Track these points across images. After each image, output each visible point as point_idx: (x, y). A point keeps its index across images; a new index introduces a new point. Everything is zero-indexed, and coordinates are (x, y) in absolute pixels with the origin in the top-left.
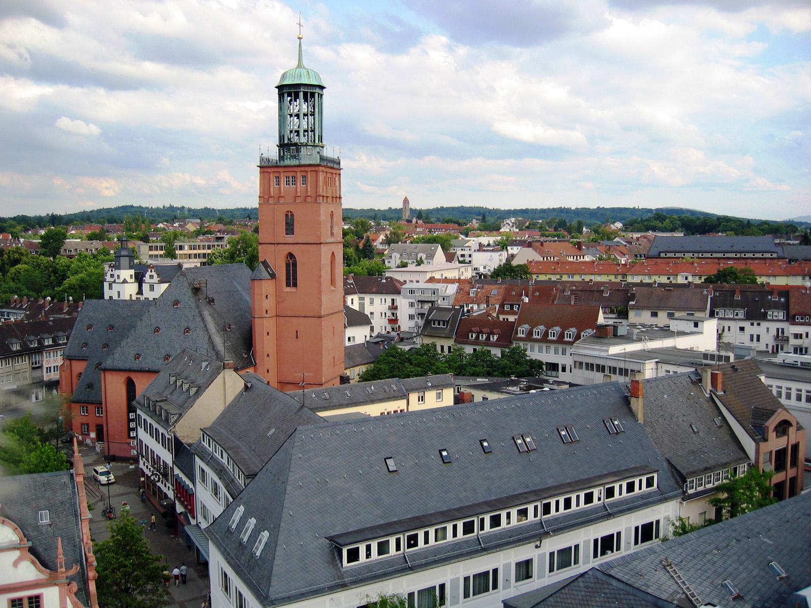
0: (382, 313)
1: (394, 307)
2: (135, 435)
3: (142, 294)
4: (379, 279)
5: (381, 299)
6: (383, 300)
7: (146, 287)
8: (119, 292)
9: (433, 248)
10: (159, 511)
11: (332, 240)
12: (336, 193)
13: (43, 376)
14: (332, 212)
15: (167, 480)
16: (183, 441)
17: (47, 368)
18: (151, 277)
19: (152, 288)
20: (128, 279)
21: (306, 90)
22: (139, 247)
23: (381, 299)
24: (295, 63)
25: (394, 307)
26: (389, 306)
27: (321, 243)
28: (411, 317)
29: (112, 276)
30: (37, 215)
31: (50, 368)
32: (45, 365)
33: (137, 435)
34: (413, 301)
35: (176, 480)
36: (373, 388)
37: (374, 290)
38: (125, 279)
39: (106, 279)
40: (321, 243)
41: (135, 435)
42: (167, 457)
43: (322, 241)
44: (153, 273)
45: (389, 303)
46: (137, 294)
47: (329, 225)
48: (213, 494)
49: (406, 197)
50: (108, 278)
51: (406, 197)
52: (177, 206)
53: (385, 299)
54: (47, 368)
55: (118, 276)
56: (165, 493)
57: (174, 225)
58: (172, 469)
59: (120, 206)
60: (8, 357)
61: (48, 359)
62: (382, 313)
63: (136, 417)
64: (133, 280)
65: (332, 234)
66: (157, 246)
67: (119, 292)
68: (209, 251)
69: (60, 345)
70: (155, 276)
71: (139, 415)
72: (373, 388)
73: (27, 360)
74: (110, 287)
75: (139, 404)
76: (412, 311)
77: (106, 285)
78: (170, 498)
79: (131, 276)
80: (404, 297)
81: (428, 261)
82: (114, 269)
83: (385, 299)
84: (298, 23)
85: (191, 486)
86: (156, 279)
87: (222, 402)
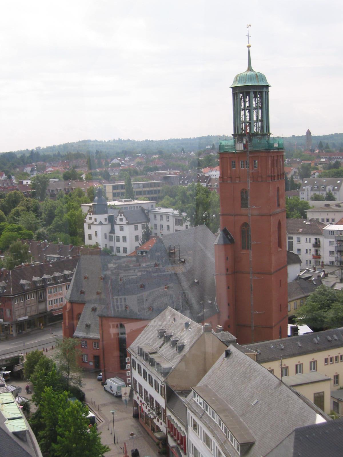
0: (307, 250)
1: (317, 245)
2: (130, 375)
3: (114, 233)
4: (304, 222)
5: (307, 239)
6: (308, 240)
7: (117, 228)
8: (96, 232)
9: (339, 182)
10: (155, 442)
11: (278, 210)
12: (281, 171)
13: (46, 308)
14: (278, 188)
15: (160, 417)
16: (173, 389)
17: (49, 301)
18: (121, 220)
19: (122, 229)
20: (104, 222)
21: (256, 90)
22: (105, 187)
23: (307, 239)
24: (246, 67)
25: (317, 245)
26: (313, 244)
27: (270, 215)
28: (331, 253)
29: (90, 219)
30: (19, 150)
31: (52, 301)
32: (48, 299)
33: (131, 374)
34: (333, 240)
35: (169, 421)
36: (318, 338)
37: (300, 231)
38: (101, 222)
39: (85, 221)
40: (270, 215)
41: (130, 375)
42: (161, 401)
43: (271, 214)
44: (123, 217)
45: (313, 241)
46: (111, 233)
47: (276, 199)
48: (205, 443)
49: (308, 130)
50: (87, 220)
51: (308, 130)
52: (124, 139)
53: (310, 239)
54: (49, 301)
55: (96, 220)
56: (157, 426)
57: (126, 159)
58: (165, 411)
59: (81, 141)
60: (21, 295)
61: (56, 304)
62: (307, 250)
63: (131, 360)
64: (107, 222)
65: (279, 205)
66: (134, 207)
67: (96, 232)
68: (159, 188)
69: (58, 283)
70: (124, 219)
71: (133, 360)
72: (318, 338)
73: (35, 296)
74: (89, 228)
75: (133, 351)
76: (333, 249)
77: (86, 226)
78: (162, 432)
79: (105, 219)
80: (326, 237)
81: (335, 192)
82: (91, 214)
83: (310, 239)
84: (250, 37)
85: (183, 429)
86: (125, 222)
87: (266, 454)
